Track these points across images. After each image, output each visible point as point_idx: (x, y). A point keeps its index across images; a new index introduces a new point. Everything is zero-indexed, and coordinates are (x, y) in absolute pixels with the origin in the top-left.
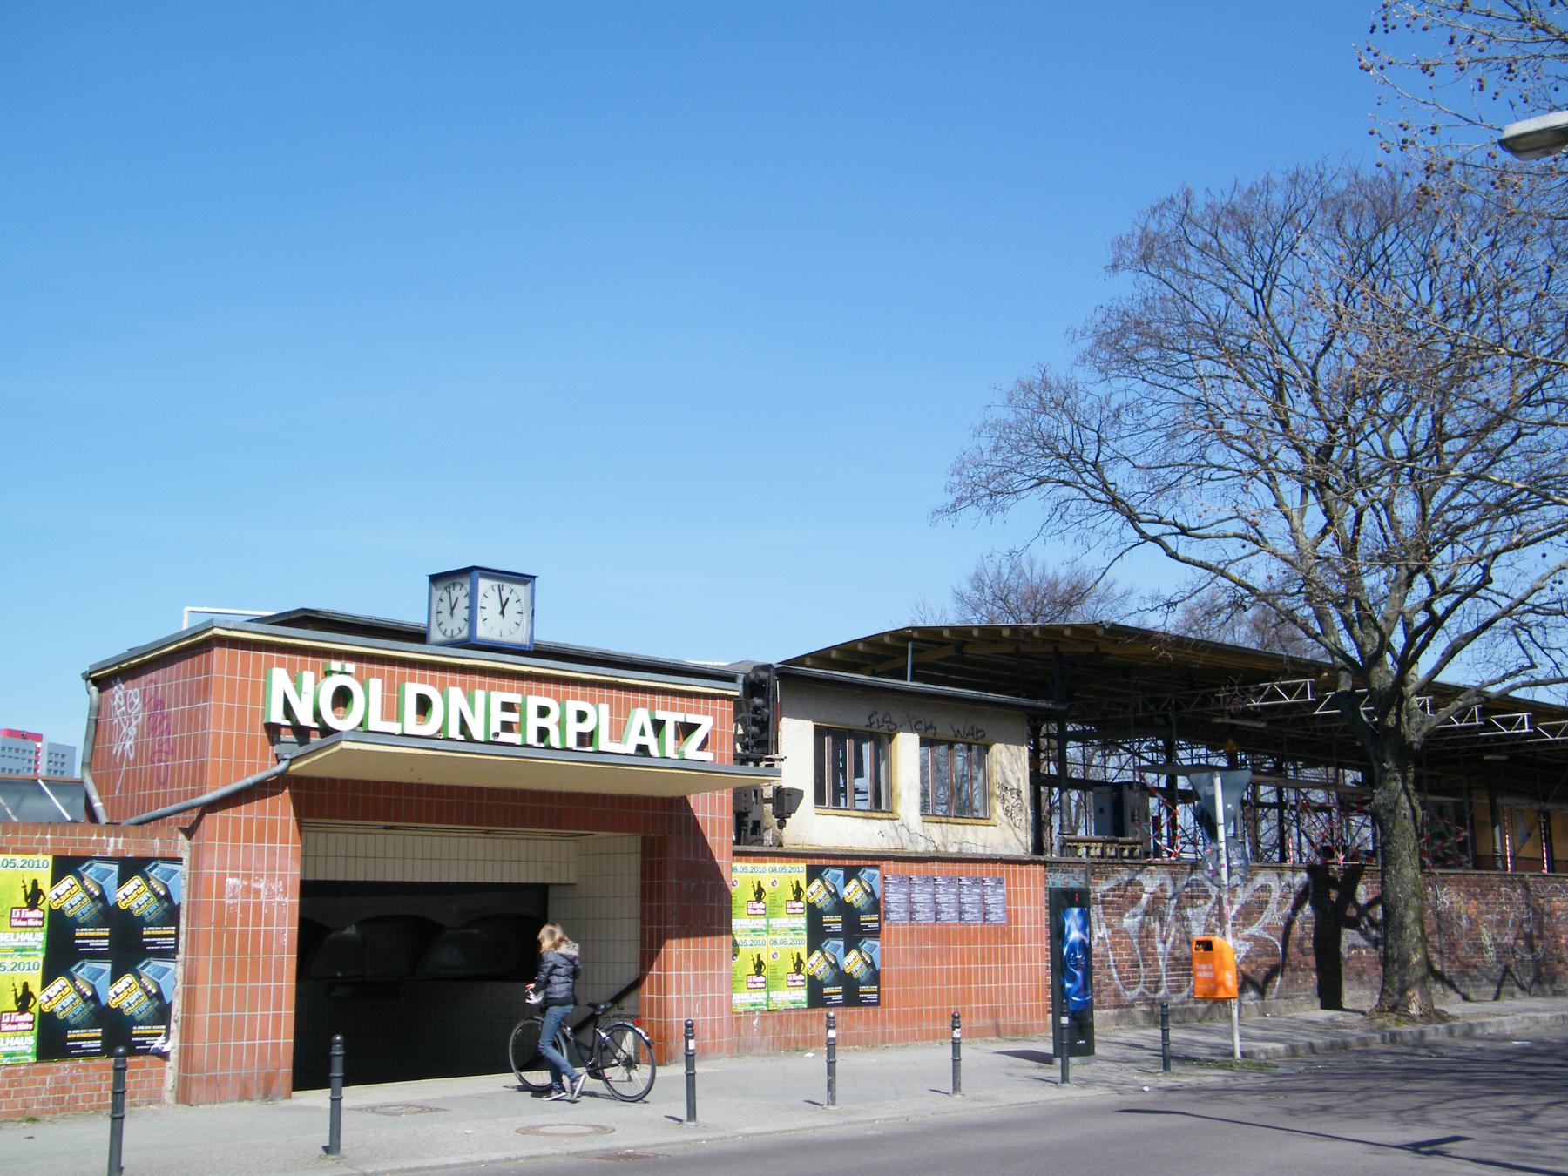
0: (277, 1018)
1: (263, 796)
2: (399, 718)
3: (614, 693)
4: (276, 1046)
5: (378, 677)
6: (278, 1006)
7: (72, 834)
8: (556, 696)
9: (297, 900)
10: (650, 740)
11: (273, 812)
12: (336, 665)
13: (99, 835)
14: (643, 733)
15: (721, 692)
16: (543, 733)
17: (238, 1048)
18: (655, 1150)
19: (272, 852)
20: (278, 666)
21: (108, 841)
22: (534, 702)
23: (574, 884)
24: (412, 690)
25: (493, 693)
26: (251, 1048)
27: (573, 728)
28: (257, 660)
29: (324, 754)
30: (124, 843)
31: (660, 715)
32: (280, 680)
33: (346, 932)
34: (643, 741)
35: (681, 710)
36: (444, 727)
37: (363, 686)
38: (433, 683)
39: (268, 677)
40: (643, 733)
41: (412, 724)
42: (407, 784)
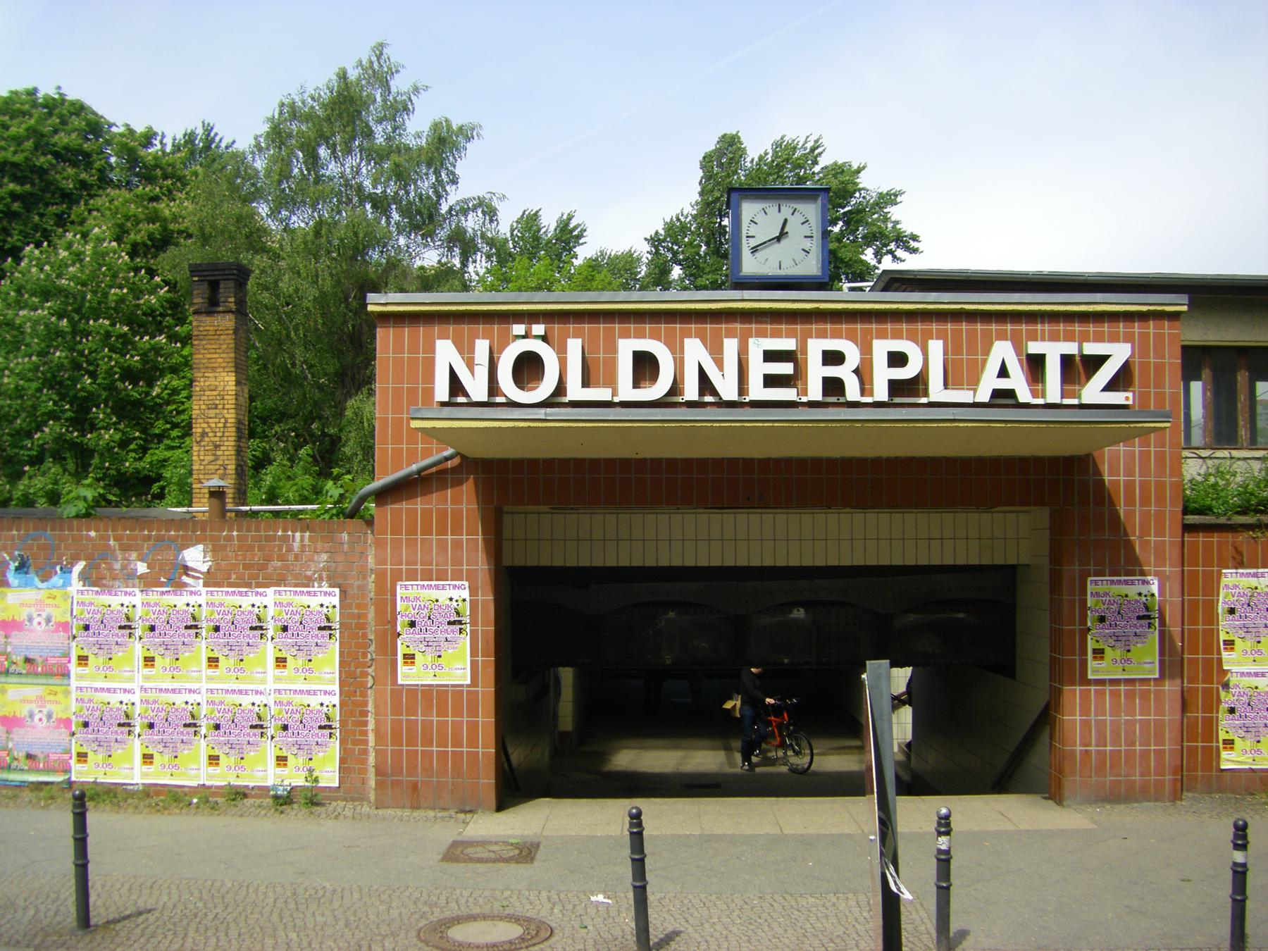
0: (473, 726)
1: (443, 486)
2: (611, 382)
3: (1137, 328)
4: (473, 756)
5: (484, 338)
6: (473, 712)
7: (258, 530)
8: (912, 337)
9: (491, 598)
10: (1018, 382)
11: (456, 500)
12: (519, 329)
13: (285, 530)
14: (1003, 373)
15: (1152, 308)
16: (833, 386)
17: (443, 755)
19: (457, 545)
20: (999, 338)
21: (294, 536)
22: (816, 348)
23: (1028, 565)
24: (627, 348)
25: (810, 342)
26: (443, 755)
27: (883, 375)
28: (972, 336)
29: (999, 425)
30: (311, 537)
31: (1034, 348)
32: (446, 353)
33: (792, 616)
34: (1003, 384)
35: (1069, 338)
36: (675, 389)
37: (673, 352)
39: (432, 349)
40: (1003, 373)
41: (627, 391)
42: (760, 460)
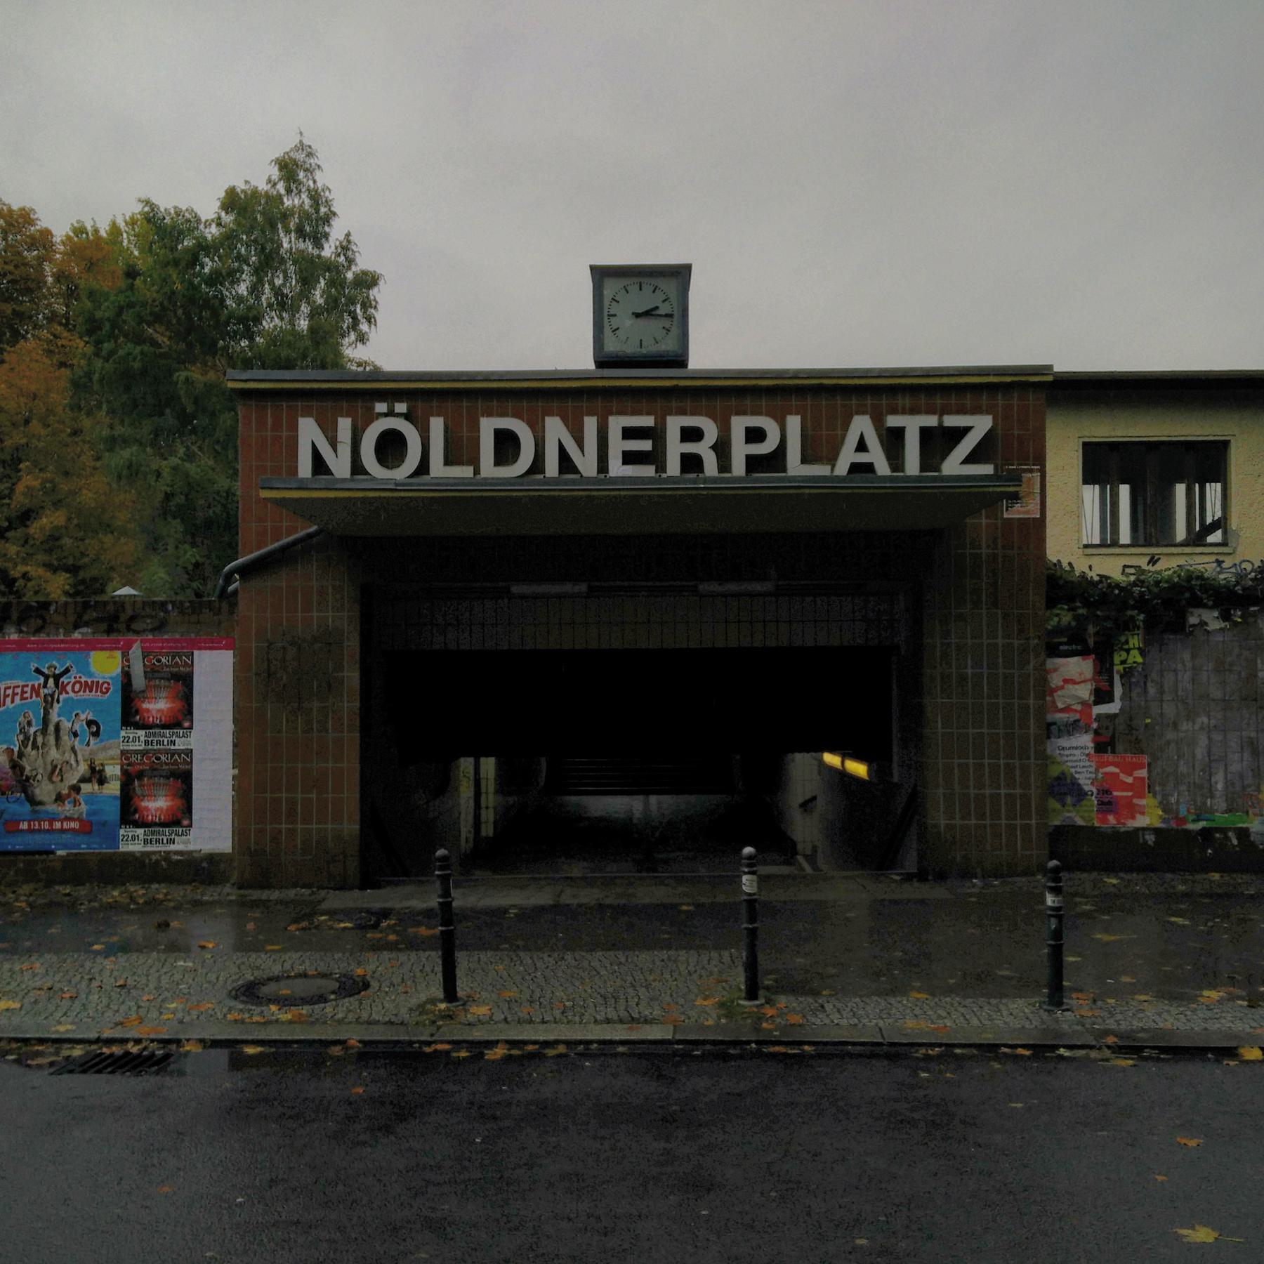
2: (475, 462)
12: (381, 407)
14: (862, 447)
18: (1061, 375)
22: (674, 425)
31: (893, 421)
32: (308, 431)
34: (862, 458)
38: (517, 415)
39: (294, 427)
40: (862, 447)
